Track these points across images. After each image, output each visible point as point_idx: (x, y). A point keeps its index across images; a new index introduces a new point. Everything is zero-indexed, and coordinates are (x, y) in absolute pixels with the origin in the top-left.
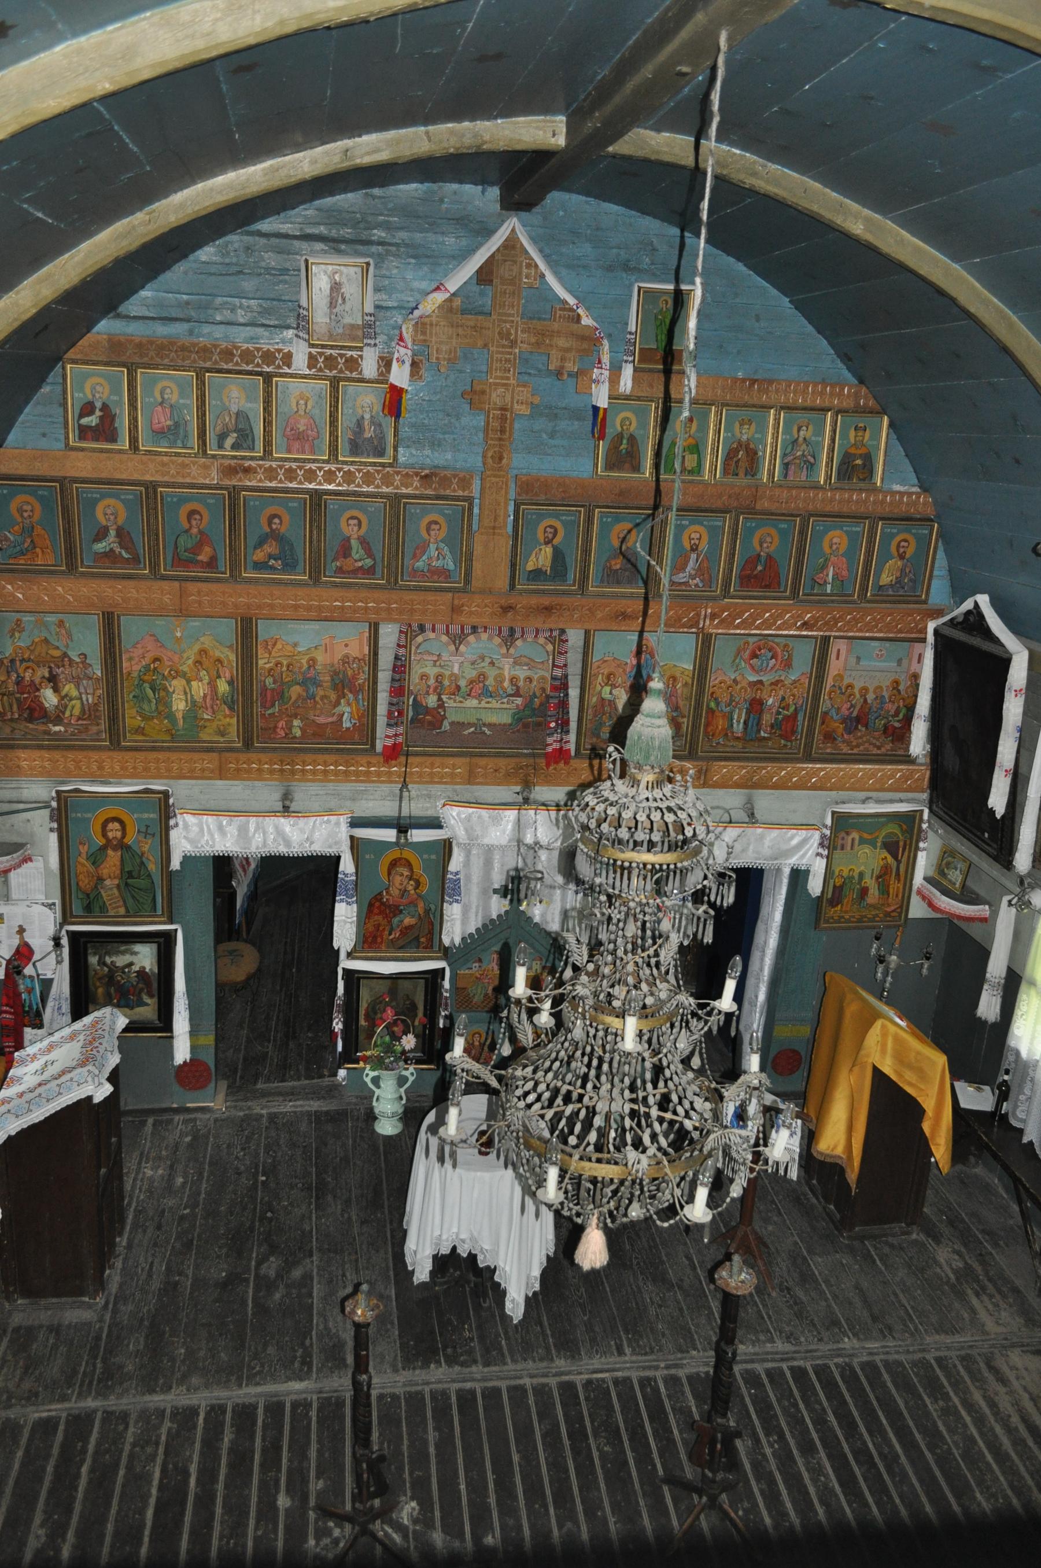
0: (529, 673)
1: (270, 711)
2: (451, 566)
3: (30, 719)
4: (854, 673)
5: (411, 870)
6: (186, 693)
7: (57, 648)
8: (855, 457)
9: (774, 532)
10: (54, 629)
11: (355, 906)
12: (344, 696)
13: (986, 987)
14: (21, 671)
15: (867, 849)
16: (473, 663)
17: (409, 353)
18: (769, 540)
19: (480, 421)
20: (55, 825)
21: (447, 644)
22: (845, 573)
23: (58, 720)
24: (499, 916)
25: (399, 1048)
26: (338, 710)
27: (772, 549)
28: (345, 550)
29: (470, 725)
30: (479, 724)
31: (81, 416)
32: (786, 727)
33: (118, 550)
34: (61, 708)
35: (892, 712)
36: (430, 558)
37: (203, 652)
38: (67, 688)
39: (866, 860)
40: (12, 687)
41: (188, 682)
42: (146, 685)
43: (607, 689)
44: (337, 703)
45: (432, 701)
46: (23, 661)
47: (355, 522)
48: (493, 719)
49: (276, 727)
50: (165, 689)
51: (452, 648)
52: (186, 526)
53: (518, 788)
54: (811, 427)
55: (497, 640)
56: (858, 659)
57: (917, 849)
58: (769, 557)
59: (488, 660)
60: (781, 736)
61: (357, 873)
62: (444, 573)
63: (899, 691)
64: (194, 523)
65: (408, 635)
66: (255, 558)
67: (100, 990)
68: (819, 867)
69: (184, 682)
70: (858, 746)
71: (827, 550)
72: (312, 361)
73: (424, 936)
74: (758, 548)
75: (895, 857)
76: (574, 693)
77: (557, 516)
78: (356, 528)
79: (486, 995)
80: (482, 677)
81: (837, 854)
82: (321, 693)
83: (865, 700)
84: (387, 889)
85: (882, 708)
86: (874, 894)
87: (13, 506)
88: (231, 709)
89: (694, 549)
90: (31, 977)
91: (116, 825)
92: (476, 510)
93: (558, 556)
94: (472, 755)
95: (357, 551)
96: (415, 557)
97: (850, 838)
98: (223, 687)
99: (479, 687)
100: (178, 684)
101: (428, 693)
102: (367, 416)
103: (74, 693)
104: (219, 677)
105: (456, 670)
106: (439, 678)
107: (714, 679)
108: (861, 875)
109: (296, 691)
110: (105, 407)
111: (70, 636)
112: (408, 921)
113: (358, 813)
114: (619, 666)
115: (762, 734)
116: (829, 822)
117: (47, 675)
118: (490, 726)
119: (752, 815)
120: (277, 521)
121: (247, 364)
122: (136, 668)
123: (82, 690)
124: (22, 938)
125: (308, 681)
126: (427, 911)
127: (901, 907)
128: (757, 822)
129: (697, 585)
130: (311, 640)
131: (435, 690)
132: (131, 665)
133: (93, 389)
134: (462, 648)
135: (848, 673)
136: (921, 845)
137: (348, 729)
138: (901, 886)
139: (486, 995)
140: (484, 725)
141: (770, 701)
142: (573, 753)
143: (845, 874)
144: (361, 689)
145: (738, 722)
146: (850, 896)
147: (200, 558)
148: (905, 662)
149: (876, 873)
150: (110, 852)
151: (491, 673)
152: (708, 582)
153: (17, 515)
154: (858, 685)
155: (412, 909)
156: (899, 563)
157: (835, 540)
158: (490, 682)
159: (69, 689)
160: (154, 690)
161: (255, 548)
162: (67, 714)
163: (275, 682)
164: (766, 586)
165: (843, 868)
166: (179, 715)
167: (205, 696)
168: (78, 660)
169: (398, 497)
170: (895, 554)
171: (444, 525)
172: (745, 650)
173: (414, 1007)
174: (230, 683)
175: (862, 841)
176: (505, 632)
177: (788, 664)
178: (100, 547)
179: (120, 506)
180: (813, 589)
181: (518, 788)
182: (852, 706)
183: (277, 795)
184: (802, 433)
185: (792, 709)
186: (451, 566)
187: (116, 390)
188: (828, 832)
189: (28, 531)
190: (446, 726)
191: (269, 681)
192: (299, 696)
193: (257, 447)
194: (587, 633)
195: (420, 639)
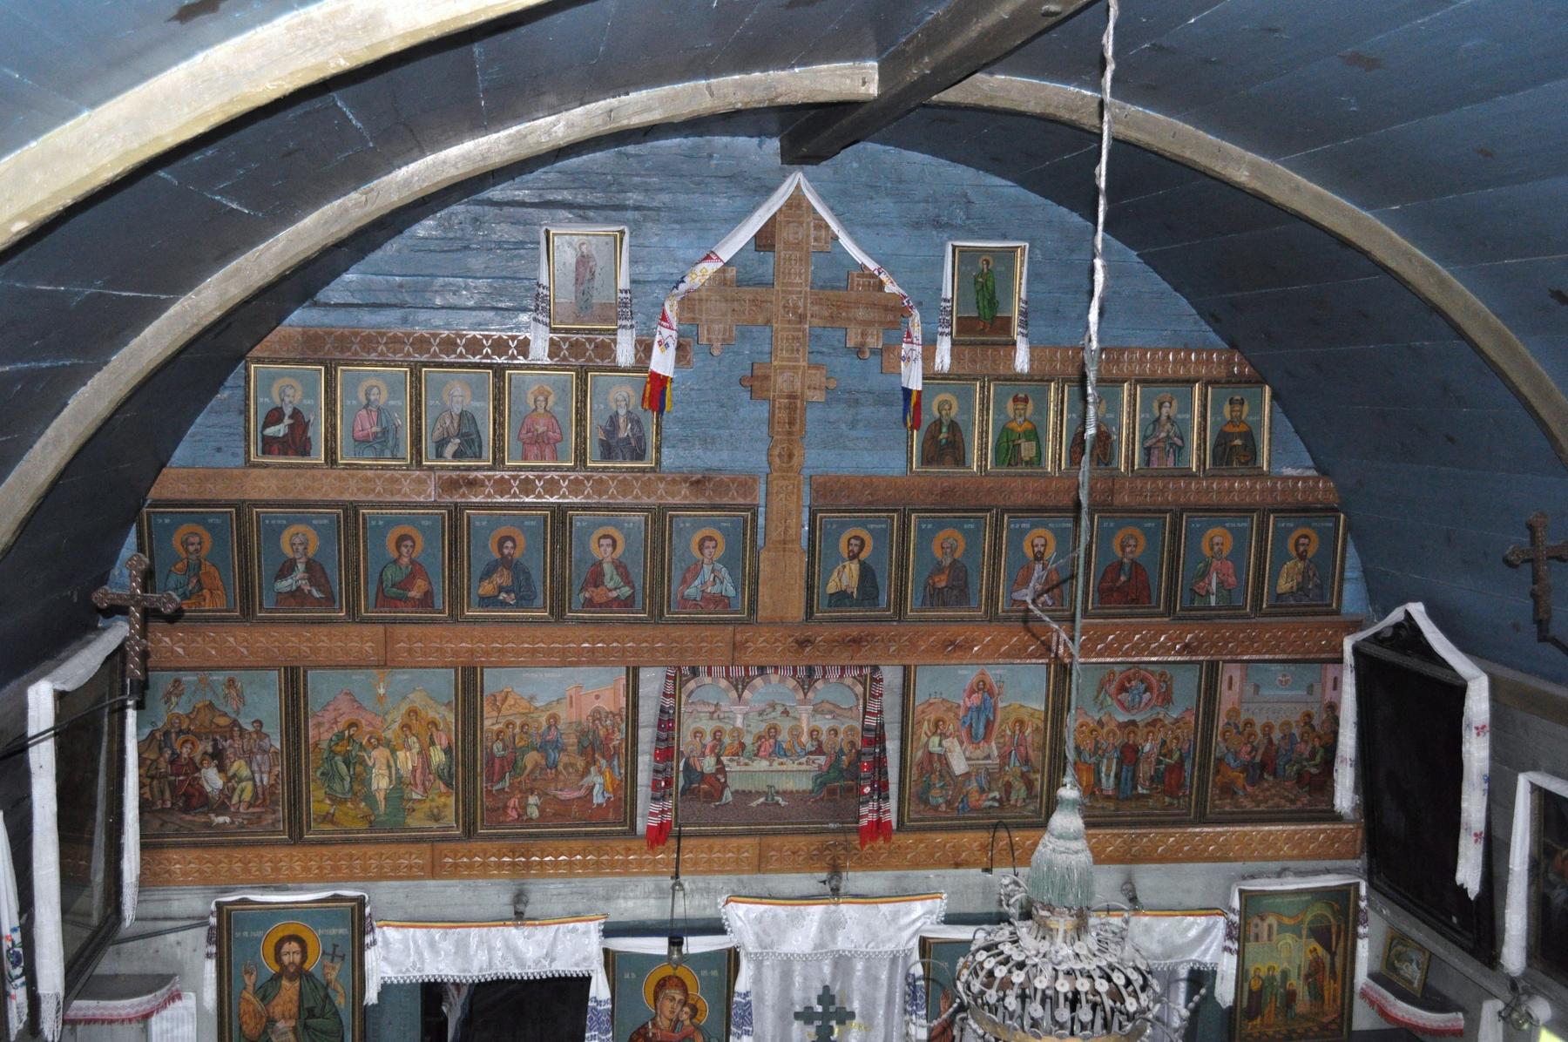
0: (833, 723)
2: (731, 592)
3: (187, 809)
6: (389, 767)
7: (225, 715)
8: (1232, 436)
9: (1138, 532)
12: (594, 762)
14: (177, 746)
19: (763, 411)
20: (213, 949)
21: (726, 691)
23: (223, 808)
26: (587, 781)
27: (1139, 550)
28: (596, 578)
29: (759, 794)
30: (770, 793)
31: (265, 426)
32: (1169, 778)
33: (307, 588)
34: (227, 792)
35: (1306, 755)
36: (704, 583)
37: (413, 712)
38: (236, 765)
40: (163, 767)
41: (393, 752)
42: (339, 759)
43: (936, 739)
44: (586, 772)
45: (708, 765)
47: (609, 541)
48: (790, 785)
49: (506, 807)
50: (363, 762)
51: (734, 694)
52: (394, 554)
53: (824, 875)
54: (1175, 403)
55: (792, 683)
56: (1257, 687)
57: (1356, 936)
58: (1134, 563)
59: (780, 709)
60: (1165, 792)
62: (721, 601)
64: (404, 550)
65: (677, 681)
66: (481, 592)
68: (1227, 966)
69: (387, 752)
71: (1207, 552)
74: (1120, 554)
76: (892, 746)
77: (864, 525)
78: (610, 549)
80: (773, 730)
82: (565, 759)
83: (1270, 741)
84: (653, 1019)
89: (1039, 557)
91: (294, 946)
92: (761, 521)
93: (866, 573)
96: (685, 582)
98: (438, 756)
99: (770, 744)
100: (379, 755)
101: (703, 755)
102: (622, 412)
103: (245, 772)
104: (433, 743)
105: (739, 723)
106: (718, 735)
108: (1285, 974)
109: (531, 758)
110: (296, 414)
111: (241, 697)
113: (614, 917)
114: (949, 710)
115: (1140, 790)
116: (1236, 903)
117: (210, 750)
118: (784, 794)
119: (1133, 899)
122: (326, 736)
123: (255, 768)
131: (712, 750)
133: (282, 392)
134: (747, 694)
135: (1245, 706)
136: (1361, 930)
137: (599, 805)
138: (1338, 986)
143: (1263, 973)
145: (1108, 776)
147: (412, 594)
150: (285, 983)
151: (785, 725)
154: (1259, 721)
156: (1300, 565)
157: (1216, 540)
158: (784, 736)
159: (239, 767)
160: (347, 763)
161: (481, 579)
162: (235, 799)
166: (381, 796)
167: (414, 769)
168: (250, 728)
170: (1294, 554)
174: (448, 751)
177: (1167, 699)
178: (285, 585)
181: (824, 875)
182: (1254, 749)
183: (507, 898)
184: (1164, 410)
185: (1176, 756)
186: (731, 592)
187: (311, 393)
188: (1236, 919)
190: (728, 796)
192: (537, 765)
195: (692, 685)
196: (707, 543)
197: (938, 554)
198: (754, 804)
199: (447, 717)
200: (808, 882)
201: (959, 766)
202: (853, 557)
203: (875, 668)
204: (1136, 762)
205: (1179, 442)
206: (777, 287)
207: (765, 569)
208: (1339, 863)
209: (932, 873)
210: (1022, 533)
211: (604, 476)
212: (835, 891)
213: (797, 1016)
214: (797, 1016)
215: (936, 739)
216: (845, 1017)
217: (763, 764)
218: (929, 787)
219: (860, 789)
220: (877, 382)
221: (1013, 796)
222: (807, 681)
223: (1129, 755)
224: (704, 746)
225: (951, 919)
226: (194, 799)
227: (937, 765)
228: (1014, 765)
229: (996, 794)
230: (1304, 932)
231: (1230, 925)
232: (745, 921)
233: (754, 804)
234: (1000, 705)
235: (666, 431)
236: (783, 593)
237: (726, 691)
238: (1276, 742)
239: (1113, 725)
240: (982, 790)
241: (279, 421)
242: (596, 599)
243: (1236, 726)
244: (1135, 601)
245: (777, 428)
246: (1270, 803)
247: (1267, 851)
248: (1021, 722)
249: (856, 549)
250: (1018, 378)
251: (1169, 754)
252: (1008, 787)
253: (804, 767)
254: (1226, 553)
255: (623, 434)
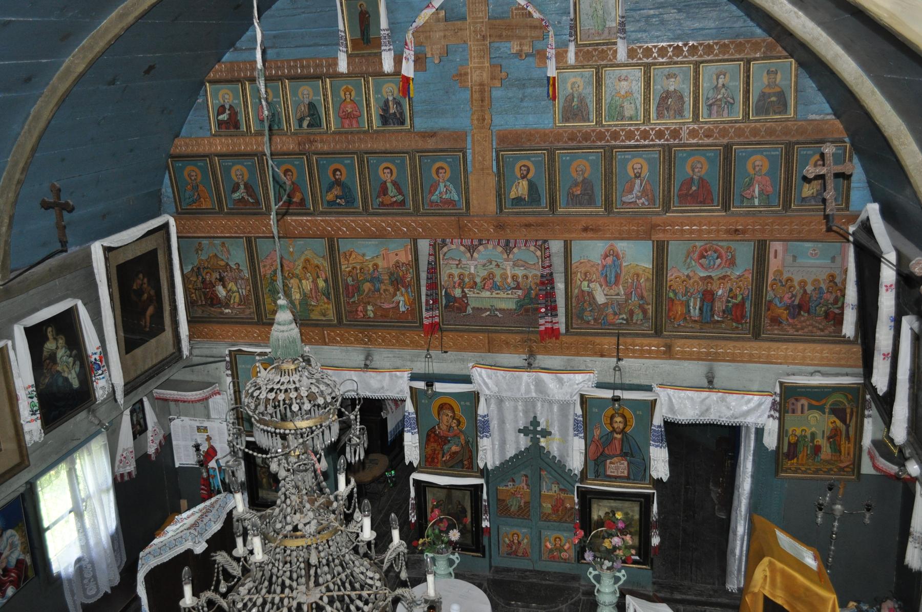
0: (525, 272)
1: (352, 300)
2: (456, 198)
3: (212, 305)
4: (792, 269)
5: (453, 412)
8: (770, 95)
9: (702, 159)
10: (220, 248)
11: (417, 436)
13: (910, 539)
14: (204, 275)
15: (816, 414)
16: (484, 266)
17: (413, 53)
18: (194, 174)
19: (467, 95)
20: (229, 372)
21: (464, 253)
22: (769, 189)
23: (227, 306)
24: (526, 449)
25: (446, 539)
27: (704, 171)
28: (384, 190)
29: (486, 310)
30: (492, 309)
31: (218, 114)
32: (735, 312)
33: (246, 197)
34: (228, 298)
35: (831, 300)
36: (441, 193)
37: (307, 260)
39: (816, 424)
40: (199, 285)
41: (300, 281)
43: (586, 283)
44: (395, 295)
45: (458, 293)
46: (204, 268)
48: (503, 305)
51: (468, 255)
53: (525, 357)
55: (500, 249)
57: (863, 416)
59: (494, 263)
60: (732, 320)
61: (417, 413)
62: (451, 202)
63: (836, 284)
65: (436, 248)
66: (328, 198)
67: (264, 480)
68: (772, 426)
70: (802, 329)
71: (752, 172)
72: (631, 53)
73: (465, 461)
74: (691, 173)
75: (843, 421)
76: (560, 286)
77: (528, 158)
78: (389, 175)
79: (520, 506)
80: (491, 276)
81: (789, 417)
82: (384, 287)
83: (805, 291)
85: (821, 298)
86: (826, 452)
87: (186, 173)
88: (328, 298)
89: (638, 176)
90: (214, 469)
92: (469, 158)
93: (532, 186)
94: (488, 331)
95: (392, 191)
96: (431, 193)
97: (799, 404)
98: (321, 284)
99: (489, 282)
101: (454, 287)
102: (390, 98)
103: (235, 289)
104: (318, 277)
105: (472, 271)
106: (461, 276)
107: (672, 275)
108: (813, 435)
109: (367, 286)
110: (231, 107)
111: (228, 251)
112: (454, 448)
115: (716, 318)
116: (778, 390)
118: (500, 310)
119: (710, 382)
120: (338, 173)
121: (603, 60)
124: (209, 443)
125: (373, 280)
126: (467, 442)
127: (853, 464)
128: (714, 388)
129: (643, 204)
130: (374, 254)
132: (265, 270)
133: (223, 97)
134: (475, 255)
135: (787, 269)
136: (866, 412)
138: (852, 445)
139: (520, 506)
140: (497, 310)
141: (720, 292)
142: (563, 329)
143: (798, 433)
144: (409, 285)
145: (695, 308)
146: (804, 453)
147: (294, 200)
148: (838, 260)
149: (827, 434)
151: (498, 272)
152: (652, 201)
153: (188, 179)
154: (797, 279)
155: (456, 439)
157: (757, 163)
158: (498, 279)
159: (231, 285)
162: (232, 301)
163: (353, 280)
164: (701, 202)
165: (796, 428)
166: (297, 303)
167: (311, 290)
169: (670, 147)
171: (448, 171)
172: (694, 252)
173: (464, 511)
174: (326, 281)
175: (811, 407)
176: (503, 242)
177: (732, 263)
178: (236, 196)
179: (588, 164)
180: (742, 202)
181: (525, 357)
182: (793, 296)
183: (362, 357)
184: (721, 81)
187: (236, 96)
188: (778, 399)
189: (195, 188)
190: (469, 310)
191: (350, 280)
192: (370, 290)
193: (686, 113)
194: (566, 242)
195: (445, 249)
196: (441, 171)
197: (574, 175)
198: (484, 315)
199: (326, 264)
200: (518, 359)
201: (601, 299)
202: (523, 178)
203: (545, 241)
204: (712, 301)
205: (732, 101)
206: (468, 21)
207: (473, 184)
208: (849, 370)
209: (588, 359)
210: (626, 161)
211: (632, 128)
212: (530, 365)
213: (520, 431)
214: (520, 431)
215: (586, 283)
216: (546, 433)
217: (487, 294)
218: (584, 310)
219: (538, 309)
220: (536, 74)
221: (635, 318)
222: (508, 248)
223: (708, 297)
224: (455, 283)
225: (600, 386)
226: (214, 300)
227: (587, 298)
228: (634, 298)
229: (624, 316)
230: (827, 410)
231: (774, 403)
232: (485, 380)
233: (484, 315)
234: (624, 264)
235: (415, 109)
236: (483, 199)
237: (464, 253)
238: (809, 292)
239: (696, 279)
240: (615, 314)
241: (224, 112)
242: (385, 202)
243: (781, 281)
244: (703, 203)
245: (475, 103)
246: (806, 330)
247: (786, 361)
248: (638, 275)
249: (525, 173)
250: (342, 75)
251: (735, 297)
252: (631, 313)
253: (510, 296)
254: (764, 172)
255: (392, 111)
